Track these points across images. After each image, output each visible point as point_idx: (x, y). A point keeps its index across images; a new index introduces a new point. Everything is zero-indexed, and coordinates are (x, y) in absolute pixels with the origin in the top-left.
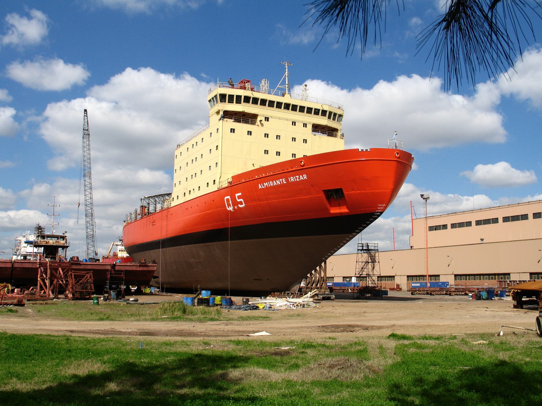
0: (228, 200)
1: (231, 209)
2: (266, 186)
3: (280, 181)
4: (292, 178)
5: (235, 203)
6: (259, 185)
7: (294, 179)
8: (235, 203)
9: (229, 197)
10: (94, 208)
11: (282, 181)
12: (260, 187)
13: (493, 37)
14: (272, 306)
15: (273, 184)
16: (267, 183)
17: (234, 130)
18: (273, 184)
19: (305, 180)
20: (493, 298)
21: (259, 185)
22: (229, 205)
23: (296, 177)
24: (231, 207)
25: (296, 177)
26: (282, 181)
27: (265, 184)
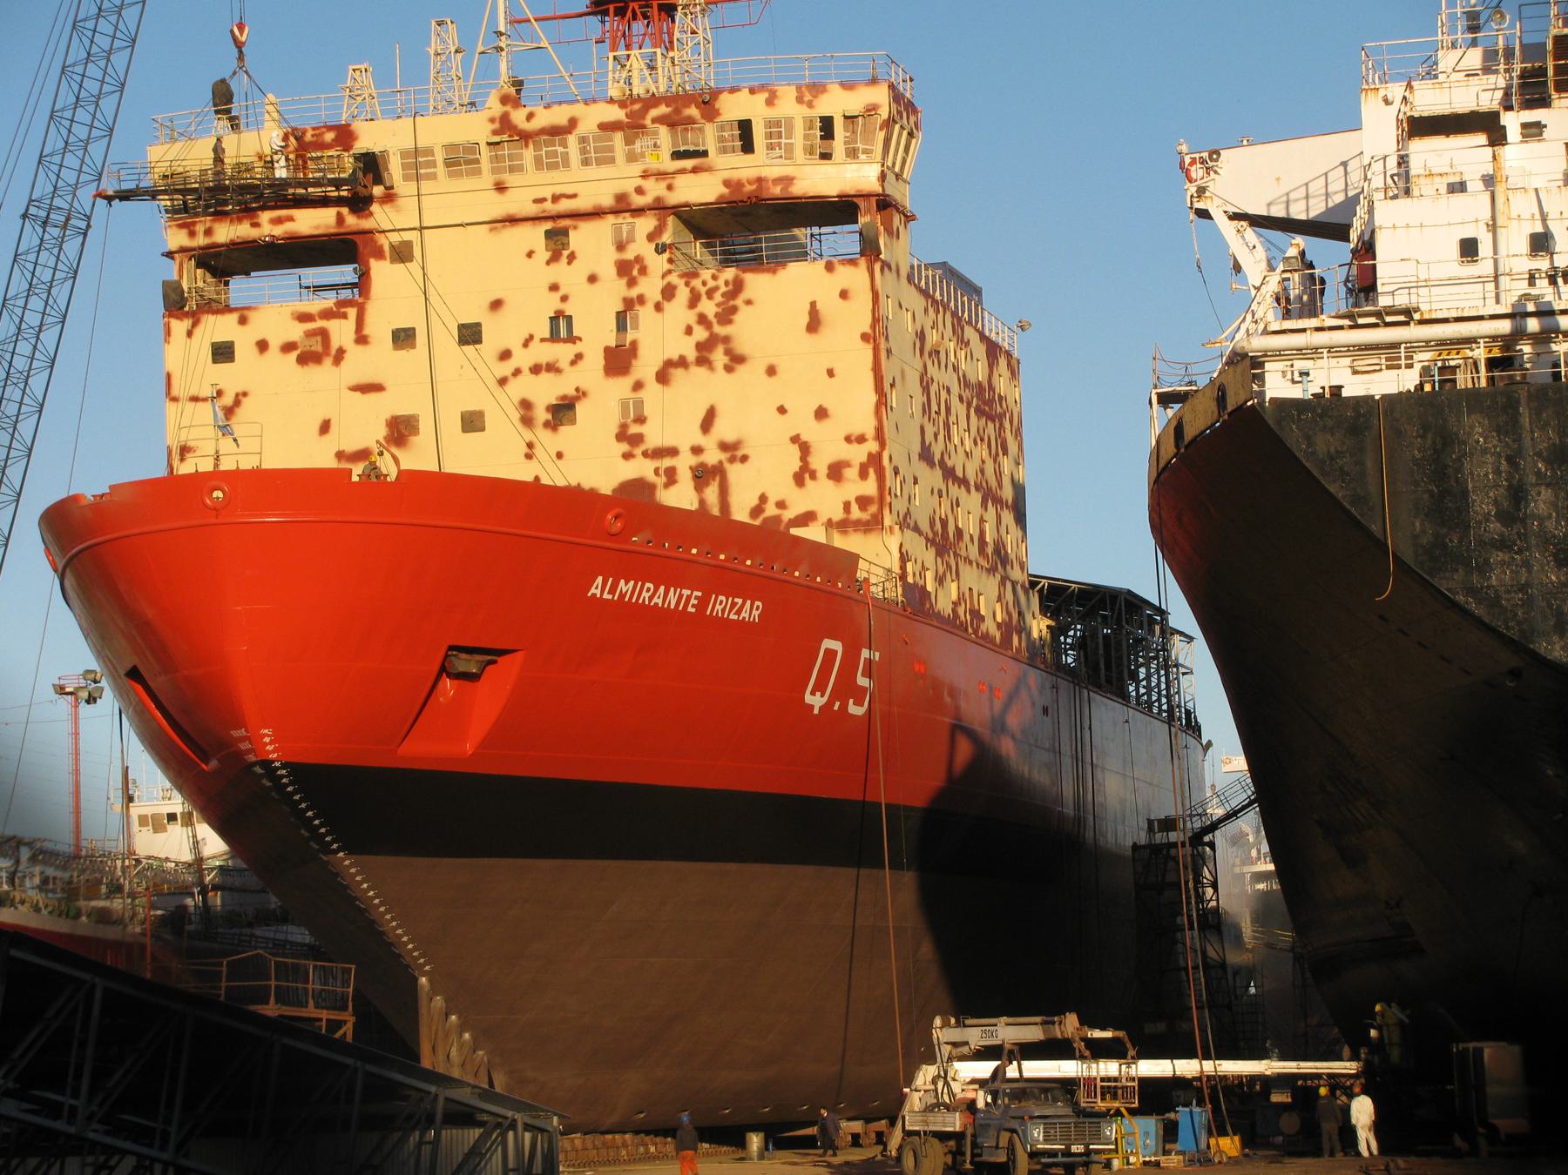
0: (831, 654)
1: (816, 701)
2: (622, 596)
3: (681, 596)
4: (648, 590)
5: (846, 689)
6: (600, 579)
7: (723, 611)
8: (846, 689)
9: (836, 646)
10: (213, 436)
11: (689, 598)
12: (593, 590)
13: (939, 456)
14: (1367, 182)
15: (651, 598)
16: (632, 583)
17: (462, 328)
18: (651, 598)
19: (751, 624)
20: (1479, 586)
21: (600, 579)
22: (820, 687)
23: (736, 600)
24: (822, 696)
25: (736, 600)
26: (689, 598)
27: (622, 582)
